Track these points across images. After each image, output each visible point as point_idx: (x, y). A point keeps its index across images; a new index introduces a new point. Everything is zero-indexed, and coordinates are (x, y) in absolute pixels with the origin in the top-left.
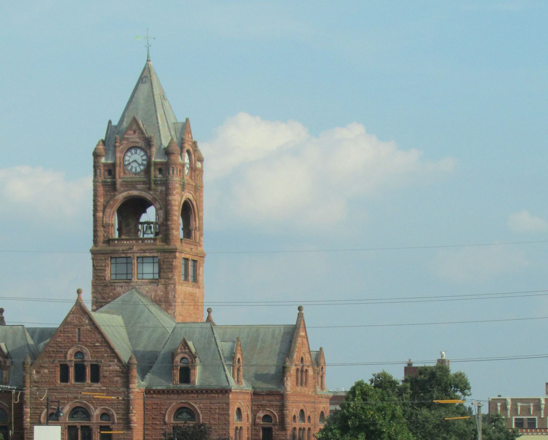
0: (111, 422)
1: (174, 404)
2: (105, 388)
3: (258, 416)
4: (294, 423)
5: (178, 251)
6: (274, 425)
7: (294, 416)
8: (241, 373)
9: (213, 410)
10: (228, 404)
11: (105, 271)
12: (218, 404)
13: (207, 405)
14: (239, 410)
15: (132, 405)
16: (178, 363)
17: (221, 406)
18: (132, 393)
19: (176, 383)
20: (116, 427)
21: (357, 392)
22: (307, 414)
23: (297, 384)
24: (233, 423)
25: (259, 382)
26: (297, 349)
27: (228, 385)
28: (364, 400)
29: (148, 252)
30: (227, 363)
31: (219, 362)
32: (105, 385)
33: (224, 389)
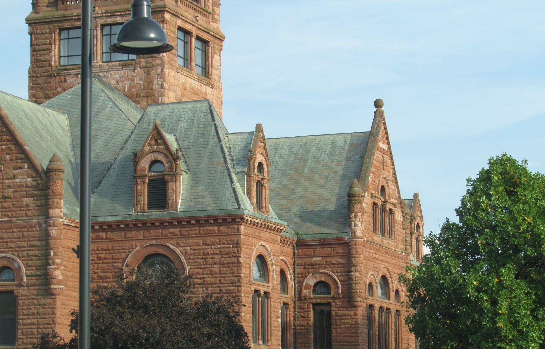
0: (16, 283)
1: (138, 248)
2: (6, 219)
3: (307, 284)
4: (370, 297)
5: (167, 9)
6: (334, 298)
7: (370, 285)
8: (266, 192)
9: (208, 257)
10: (237, 244)
11: (50, 52)
12: (220, 244)
13: (200, 247)
14: (261, 259)
15: (52, 249)
16: (145, 171)
17: (224, 248)
18: (54, 226)
19: (141, 209)
20: (25, 293)
21: (495, 178)
22: (393, 287)
23: (375, 230)
24: (249, 281)
25: (309, 224)
26: (373, 169)
27: (236, 207)
28: (510, 193)
29: (118, 15)
30: (237, 170)
31: (221, 167)
32: (6, 213)
33: (229, 215)
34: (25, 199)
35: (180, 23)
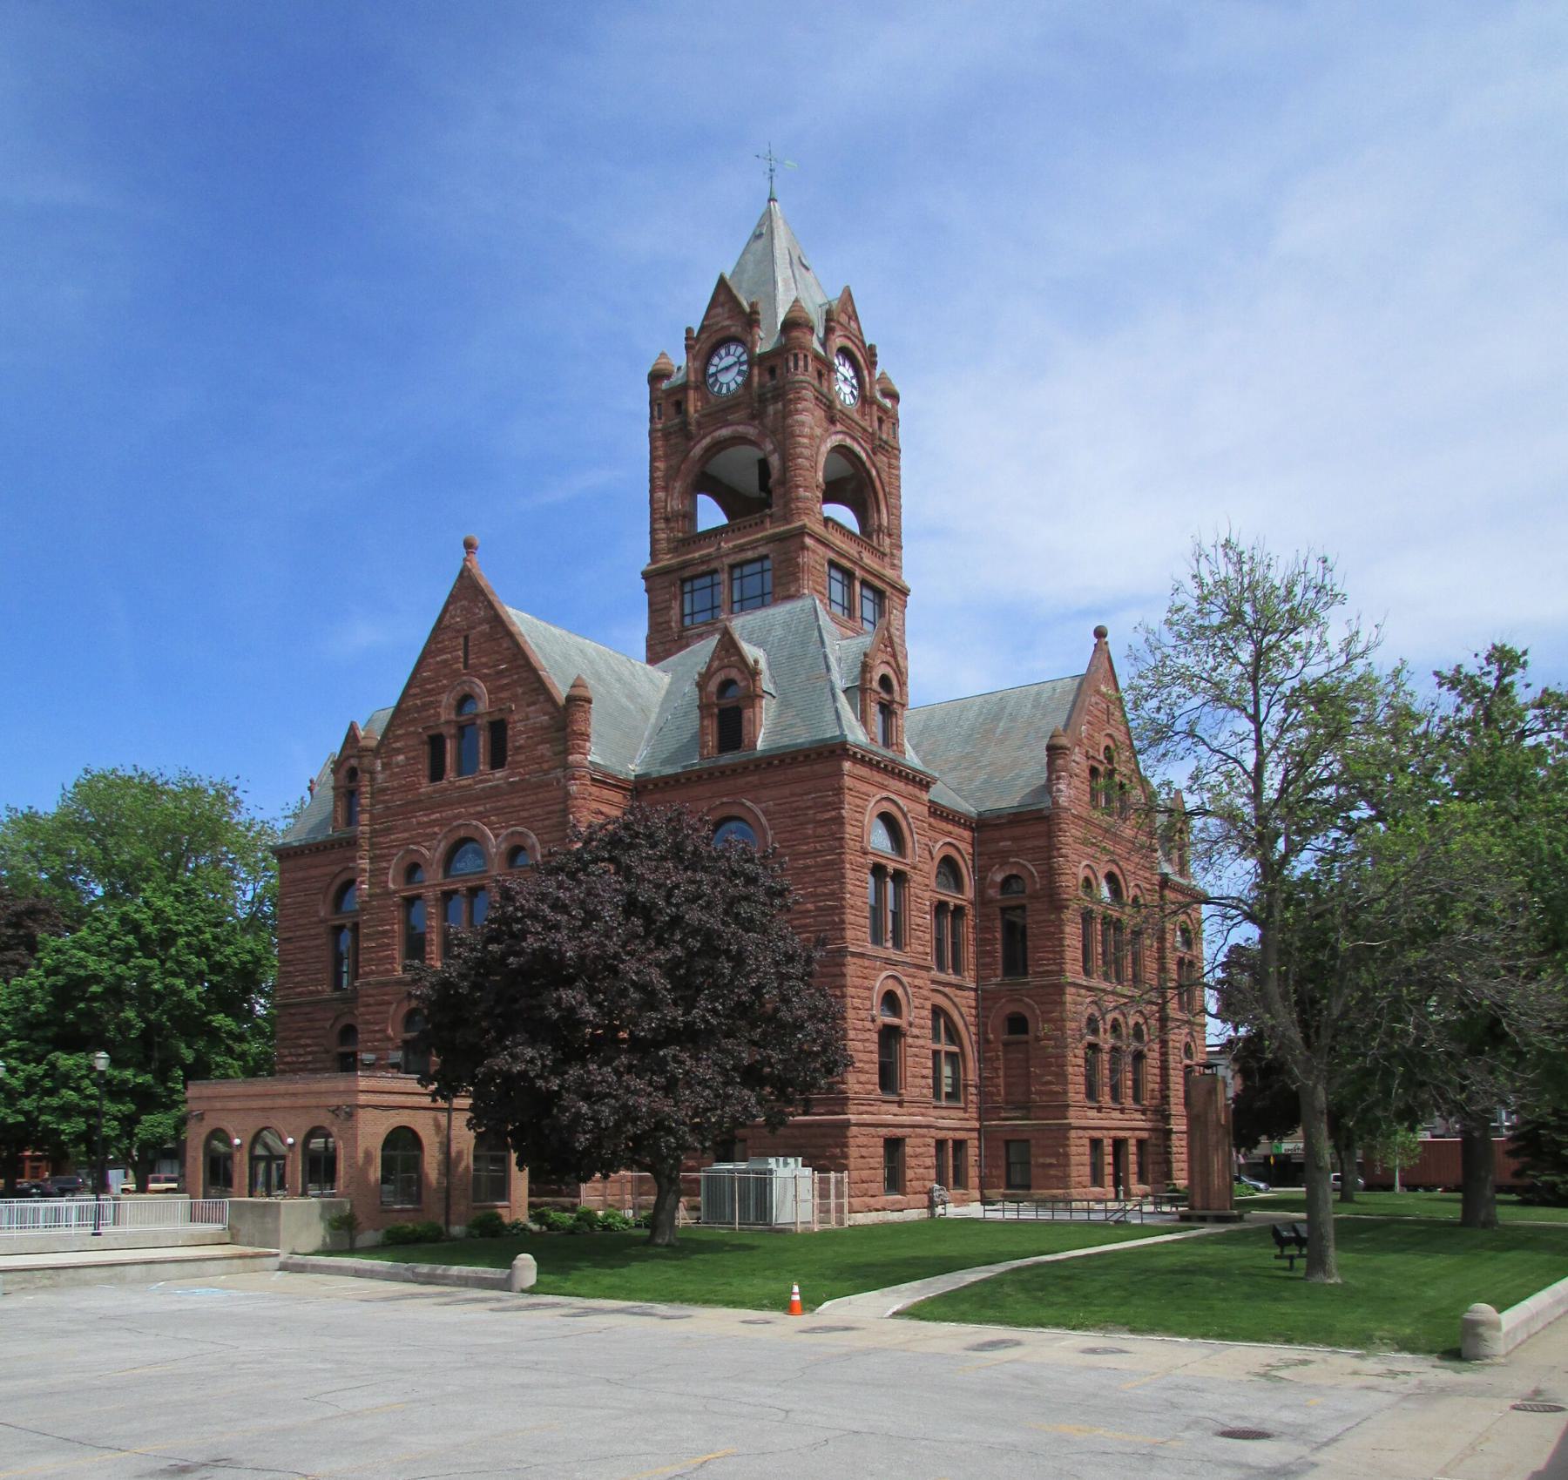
34: (540, 747)
35: (832, 555)
